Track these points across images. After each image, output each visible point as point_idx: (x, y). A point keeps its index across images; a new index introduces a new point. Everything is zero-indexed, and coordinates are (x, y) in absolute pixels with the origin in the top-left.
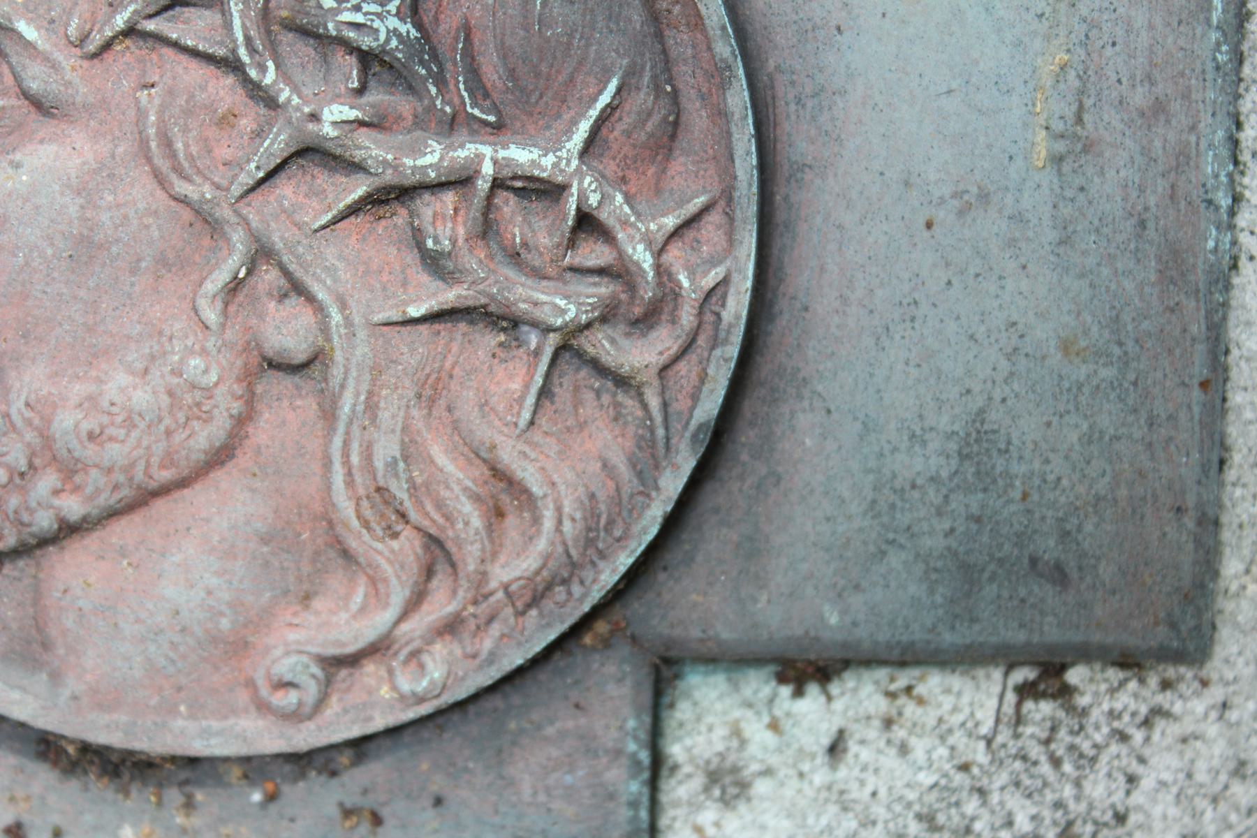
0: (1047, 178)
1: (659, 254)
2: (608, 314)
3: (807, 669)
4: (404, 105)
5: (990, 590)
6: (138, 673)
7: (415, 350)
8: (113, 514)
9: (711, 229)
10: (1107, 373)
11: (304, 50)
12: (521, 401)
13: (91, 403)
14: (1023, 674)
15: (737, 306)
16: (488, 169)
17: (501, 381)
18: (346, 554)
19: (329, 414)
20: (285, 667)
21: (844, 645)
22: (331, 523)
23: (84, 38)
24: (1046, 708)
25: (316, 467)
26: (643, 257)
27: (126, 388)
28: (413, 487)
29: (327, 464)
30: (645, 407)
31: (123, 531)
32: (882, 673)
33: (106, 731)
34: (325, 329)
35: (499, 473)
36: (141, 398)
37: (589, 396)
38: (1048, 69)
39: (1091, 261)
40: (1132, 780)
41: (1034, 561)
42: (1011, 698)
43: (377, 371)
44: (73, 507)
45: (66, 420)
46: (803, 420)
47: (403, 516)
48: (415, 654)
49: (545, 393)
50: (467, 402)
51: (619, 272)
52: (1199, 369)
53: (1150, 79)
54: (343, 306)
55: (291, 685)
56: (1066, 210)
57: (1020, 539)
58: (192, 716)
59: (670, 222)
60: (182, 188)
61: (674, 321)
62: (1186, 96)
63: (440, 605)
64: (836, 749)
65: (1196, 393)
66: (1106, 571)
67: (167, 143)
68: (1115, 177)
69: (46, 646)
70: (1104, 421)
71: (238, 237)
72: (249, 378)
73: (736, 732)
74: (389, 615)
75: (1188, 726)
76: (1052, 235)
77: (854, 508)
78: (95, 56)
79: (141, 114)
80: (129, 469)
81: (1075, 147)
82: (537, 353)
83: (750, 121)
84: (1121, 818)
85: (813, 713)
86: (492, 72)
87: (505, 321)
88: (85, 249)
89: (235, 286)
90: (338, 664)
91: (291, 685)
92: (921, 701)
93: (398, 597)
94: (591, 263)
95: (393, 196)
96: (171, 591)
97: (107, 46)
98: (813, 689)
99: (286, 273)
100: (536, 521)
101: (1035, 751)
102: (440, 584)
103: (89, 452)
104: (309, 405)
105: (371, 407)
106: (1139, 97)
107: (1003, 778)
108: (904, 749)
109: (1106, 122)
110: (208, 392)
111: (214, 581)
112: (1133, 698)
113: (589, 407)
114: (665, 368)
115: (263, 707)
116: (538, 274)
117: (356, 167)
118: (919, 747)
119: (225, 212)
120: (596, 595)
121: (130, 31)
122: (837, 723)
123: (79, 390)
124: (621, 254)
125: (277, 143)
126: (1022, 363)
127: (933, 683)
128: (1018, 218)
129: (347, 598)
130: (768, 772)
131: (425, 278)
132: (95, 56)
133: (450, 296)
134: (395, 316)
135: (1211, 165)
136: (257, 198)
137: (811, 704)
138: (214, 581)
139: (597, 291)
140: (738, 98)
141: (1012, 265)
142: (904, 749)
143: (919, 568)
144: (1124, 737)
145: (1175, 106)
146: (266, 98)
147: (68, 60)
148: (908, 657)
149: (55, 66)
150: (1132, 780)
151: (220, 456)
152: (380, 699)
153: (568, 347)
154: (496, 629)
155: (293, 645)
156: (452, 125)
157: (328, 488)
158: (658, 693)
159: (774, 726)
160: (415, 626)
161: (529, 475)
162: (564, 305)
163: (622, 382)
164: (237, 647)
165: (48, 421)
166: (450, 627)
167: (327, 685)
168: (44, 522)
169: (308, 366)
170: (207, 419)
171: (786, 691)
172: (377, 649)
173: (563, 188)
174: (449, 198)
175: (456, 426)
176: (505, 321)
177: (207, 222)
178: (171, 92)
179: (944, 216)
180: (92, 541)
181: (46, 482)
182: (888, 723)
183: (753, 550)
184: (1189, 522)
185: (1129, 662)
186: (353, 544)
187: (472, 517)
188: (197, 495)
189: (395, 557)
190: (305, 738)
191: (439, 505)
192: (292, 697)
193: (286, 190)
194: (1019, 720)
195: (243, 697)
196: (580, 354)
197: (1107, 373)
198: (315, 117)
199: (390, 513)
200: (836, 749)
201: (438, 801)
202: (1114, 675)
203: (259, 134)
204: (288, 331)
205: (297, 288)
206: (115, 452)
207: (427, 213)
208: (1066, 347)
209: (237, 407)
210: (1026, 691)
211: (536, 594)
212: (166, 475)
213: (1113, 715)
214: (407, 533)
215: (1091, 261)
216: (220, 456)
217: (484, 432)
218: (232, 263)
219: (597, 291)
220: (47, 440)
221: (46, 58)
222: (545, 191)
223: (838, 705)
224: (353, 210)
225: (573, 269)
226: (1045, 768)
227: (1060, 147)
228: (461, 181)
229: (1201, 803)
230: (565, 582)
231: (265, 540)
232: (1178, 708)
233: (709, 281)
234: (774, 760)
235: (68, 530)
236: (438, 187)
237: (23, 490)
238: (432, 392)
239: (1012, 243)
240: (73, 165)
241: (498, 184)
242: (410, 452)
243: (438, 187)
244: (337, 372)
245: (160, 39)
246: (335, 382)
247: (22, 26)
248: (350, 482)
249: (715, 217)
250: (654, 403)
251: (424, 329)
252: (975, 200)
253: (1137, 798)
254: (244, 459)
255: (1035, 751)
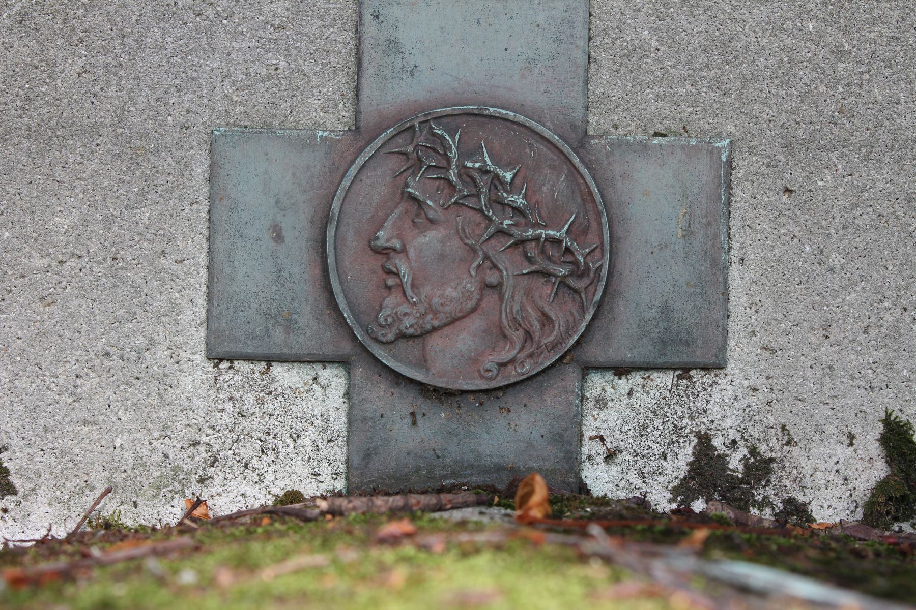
0: (682, 241)
1: (585, 258)
2: (572, 274)
3: (621, 370)
4: (522, 220)
5: (669, 348)
6: (450, 368)
7: (524, 282)
8: (446, 325)
9: (597, 253)
10: (698, 291)
11: (499, 207)
12: (550, 295)
13: (442, 296)
14: (677, 373)
15: (605, 271)
16: (544, 236)
17: (544, 290)
18: (505, 336)
19: (501, 299)
20: (488, 366)
21: (632, 363)
22: (501, 328)
23: (443, 205)
24: (685, 381)
25: (498, 313)
26: (581, 258)
27: (450, 292)
28: (523, 318)
29: (501, 312)
30: (581, 297)
31: (447, 331)
32: (642, 373)
33: (441, 383)
34: (502, 277)
35: (545, 315)
36: (455, 294)
37: (567, 295)
38: (681, 214)
39: (693, 262)
40: (708, 401)
41: (681, 340)
42: (676, 379)
43: (514, 287)
44: (436, 323)
45: (435, 300)
46: (621, 303)
47: (520, 325)
48: (522, 362)
49: (556, 294)
50: (536, 295)
51: (576, 263)
52: (721, 289)
53: (706, 216)
54: (507, 271)
55: (490, 370)
56: (687, 249)
57: (677, 334)
58: (463, 380)
59: (587, 250)
60: (467, 241)
61: (588, 275)
62: (716, 220)
63: (529, 350)
64: (630, 394)
65: (721, 296)
66: (699, 342)
67: (463, 230)
68: (698, 242)
69: (425, 361)
70: (698, 303)
71: (480, 253)
72: (482, 289)
73: (603, 389)
74: (516, 352)
75: (722, 387)
76: (684, 255)
77: (634, 326)
78: (446, 209)
79: (457, 223)
80: (450, 313)
81: (688, 233)
82: (554, 283)
83: (758, 575)
84: (705, 412)
85: (624, 384)
86: (543, 214)
87: (546, 274)
88: (442, 257)
89: (479, 266)
90: (502, 365)
91: (490, 370)
92: (652, 380)
93: (518, 347)
94: (568, 260)
95: (522, 242)
96: (460, 345)
97: (449, 206)
98: (624, 377)
99: (492, 262)
100: (554, 327)
101: (682, 394)
102: (528, 344)
103: (441, 308)
104: (496, 297)
105: (513, 297)
106: (704, 221)
107: (674, 401)
108: (648, 394)
109: (696, 227)
110: (472, 293)
111: (470, 343)
112: (708, 379)
113: (567, 298)
114: (586, 288)
115: (482, 377)
116: (555, 263)
117: (512, 236)
118: (652, 393)
119: (478, 247)
120: (569, 346)
121: (456, 203)
122: (630, 386)
123: (439, 292)
124: (576, 259)
125: (492, 229)
126: (677, 288)
127: (655, 375)
128: (674, 251)
129: (504, 348)
130: (612, 400)
131: (527, 263)
132: (446, 209)
133: (534, 268)
134: (519, 273)
135: (723, 238)
136: (485, 244)
137: (623, 382)
138: (470, 343)
139: (569, 268)
140: (604, 220)
141: (673, 263)
142: (648, 394)
143: (651, 342)
144: (705, 390)
145: (713, 223)
146: (489, 219)
147: (439, 210)
148: (647, 367)
149: (436, 211)
150: (708, 401)
151: (474, 310)
152: (513, 374)
153: (563, 283)
154: (543, 356)
155: (490, 361)
156: (536, 225)
157: (501, 317)
158: (583, 378)
159: (613, 387)
160: (521, 356)
161: (552, 315)
162: (562, 271)
163: (576, 291)
164: (475, 361)
165: (431, 301)
166: (531, 356)
167: (499, 371)
168: (428, 327)
169: (497, 287)
170: (471, 300)
171: (616, 378)
172: (512, 361)
173: (562, 241)
174: (534, 244)
175: (534, 302)
176: (546, 274)
177: (473, 250)
178: (465, 218)
179: (656, 250)
180: (439, 333)
181: (430, 316)
182: (644, 386)
183: (608, 337)
184: (720, 329)
185: (706, 368)
186: (507, 332)
187: (537, 325)
188: (466, 320)
189: (517, 336)
190: (494, 384)
191: (529, 322)
192: (490, 374)
193: (493, 242)
194: (678, 385)
195: (476, 375)
196: (565, 284)
197: (698, 291)
198: (502, 223)
199: (517, 324)
200: (630, 394)
201: (525, 405)
202: (703, 373)
203: (487, 228)
204: (492, 278)
205: (495, 267)
206: (448, 309)
207: (528, 247)
208: (687, 284)
209: (478, 297)
210: (680, 377)
211: (553, 347)
212: (460, 315)
213: (703, 384)
214: (521, 330)
215: (693, 262)
216: (474, 310)
217: (541, 303)
218: (479, 260)
219: (569, 268)
220: (430, 306)
221: (434, 210)
222: (557, 242)
223: (630, 382)
224: (510, 247)
225: (564, 262)
226: (685, 398)
227: (685, 233)
228: (537, 239)
229: (726, 408)
230: (561, 343)
231: (484, 332)
232: (719, 382)
233: (597, 265)
234: (613, 397)
235: (434, 329)
236: (532, 240)
237: (423, 319)
238: (528, 293)
239: (673, 257)
240: (440, 236)
241: (546, 240)
242: (522, 308)
243: (532, 240)
244: (504, 287)
245: (463, 205)
246: (504, 290)
247: (428, 202)
248: (507, 317)
249: (598, 250)
250: (583, 296)
251: (526, 277)
252: (664, 246)
253: (709, 406)
254: (479, 311)
255: (682, 394)
